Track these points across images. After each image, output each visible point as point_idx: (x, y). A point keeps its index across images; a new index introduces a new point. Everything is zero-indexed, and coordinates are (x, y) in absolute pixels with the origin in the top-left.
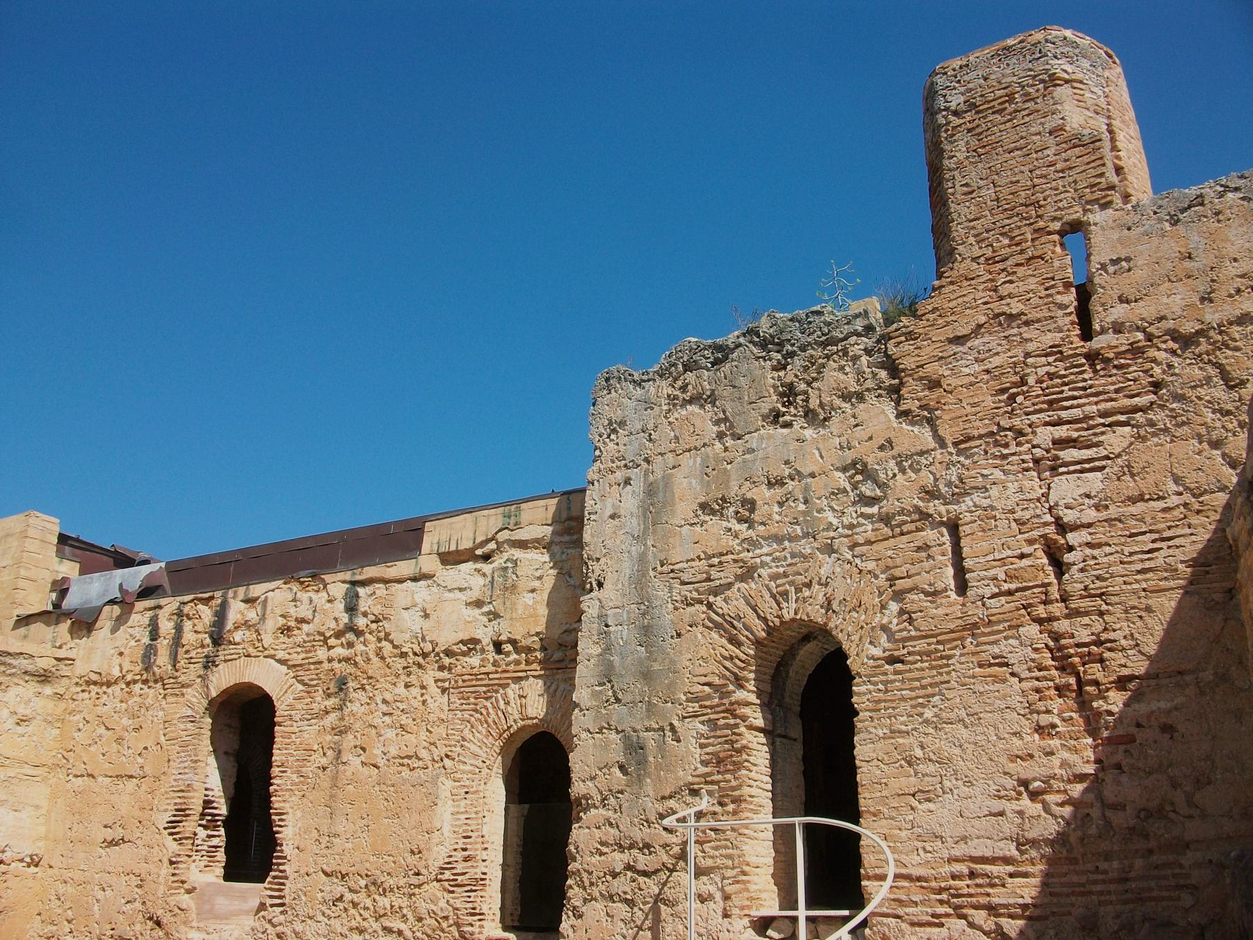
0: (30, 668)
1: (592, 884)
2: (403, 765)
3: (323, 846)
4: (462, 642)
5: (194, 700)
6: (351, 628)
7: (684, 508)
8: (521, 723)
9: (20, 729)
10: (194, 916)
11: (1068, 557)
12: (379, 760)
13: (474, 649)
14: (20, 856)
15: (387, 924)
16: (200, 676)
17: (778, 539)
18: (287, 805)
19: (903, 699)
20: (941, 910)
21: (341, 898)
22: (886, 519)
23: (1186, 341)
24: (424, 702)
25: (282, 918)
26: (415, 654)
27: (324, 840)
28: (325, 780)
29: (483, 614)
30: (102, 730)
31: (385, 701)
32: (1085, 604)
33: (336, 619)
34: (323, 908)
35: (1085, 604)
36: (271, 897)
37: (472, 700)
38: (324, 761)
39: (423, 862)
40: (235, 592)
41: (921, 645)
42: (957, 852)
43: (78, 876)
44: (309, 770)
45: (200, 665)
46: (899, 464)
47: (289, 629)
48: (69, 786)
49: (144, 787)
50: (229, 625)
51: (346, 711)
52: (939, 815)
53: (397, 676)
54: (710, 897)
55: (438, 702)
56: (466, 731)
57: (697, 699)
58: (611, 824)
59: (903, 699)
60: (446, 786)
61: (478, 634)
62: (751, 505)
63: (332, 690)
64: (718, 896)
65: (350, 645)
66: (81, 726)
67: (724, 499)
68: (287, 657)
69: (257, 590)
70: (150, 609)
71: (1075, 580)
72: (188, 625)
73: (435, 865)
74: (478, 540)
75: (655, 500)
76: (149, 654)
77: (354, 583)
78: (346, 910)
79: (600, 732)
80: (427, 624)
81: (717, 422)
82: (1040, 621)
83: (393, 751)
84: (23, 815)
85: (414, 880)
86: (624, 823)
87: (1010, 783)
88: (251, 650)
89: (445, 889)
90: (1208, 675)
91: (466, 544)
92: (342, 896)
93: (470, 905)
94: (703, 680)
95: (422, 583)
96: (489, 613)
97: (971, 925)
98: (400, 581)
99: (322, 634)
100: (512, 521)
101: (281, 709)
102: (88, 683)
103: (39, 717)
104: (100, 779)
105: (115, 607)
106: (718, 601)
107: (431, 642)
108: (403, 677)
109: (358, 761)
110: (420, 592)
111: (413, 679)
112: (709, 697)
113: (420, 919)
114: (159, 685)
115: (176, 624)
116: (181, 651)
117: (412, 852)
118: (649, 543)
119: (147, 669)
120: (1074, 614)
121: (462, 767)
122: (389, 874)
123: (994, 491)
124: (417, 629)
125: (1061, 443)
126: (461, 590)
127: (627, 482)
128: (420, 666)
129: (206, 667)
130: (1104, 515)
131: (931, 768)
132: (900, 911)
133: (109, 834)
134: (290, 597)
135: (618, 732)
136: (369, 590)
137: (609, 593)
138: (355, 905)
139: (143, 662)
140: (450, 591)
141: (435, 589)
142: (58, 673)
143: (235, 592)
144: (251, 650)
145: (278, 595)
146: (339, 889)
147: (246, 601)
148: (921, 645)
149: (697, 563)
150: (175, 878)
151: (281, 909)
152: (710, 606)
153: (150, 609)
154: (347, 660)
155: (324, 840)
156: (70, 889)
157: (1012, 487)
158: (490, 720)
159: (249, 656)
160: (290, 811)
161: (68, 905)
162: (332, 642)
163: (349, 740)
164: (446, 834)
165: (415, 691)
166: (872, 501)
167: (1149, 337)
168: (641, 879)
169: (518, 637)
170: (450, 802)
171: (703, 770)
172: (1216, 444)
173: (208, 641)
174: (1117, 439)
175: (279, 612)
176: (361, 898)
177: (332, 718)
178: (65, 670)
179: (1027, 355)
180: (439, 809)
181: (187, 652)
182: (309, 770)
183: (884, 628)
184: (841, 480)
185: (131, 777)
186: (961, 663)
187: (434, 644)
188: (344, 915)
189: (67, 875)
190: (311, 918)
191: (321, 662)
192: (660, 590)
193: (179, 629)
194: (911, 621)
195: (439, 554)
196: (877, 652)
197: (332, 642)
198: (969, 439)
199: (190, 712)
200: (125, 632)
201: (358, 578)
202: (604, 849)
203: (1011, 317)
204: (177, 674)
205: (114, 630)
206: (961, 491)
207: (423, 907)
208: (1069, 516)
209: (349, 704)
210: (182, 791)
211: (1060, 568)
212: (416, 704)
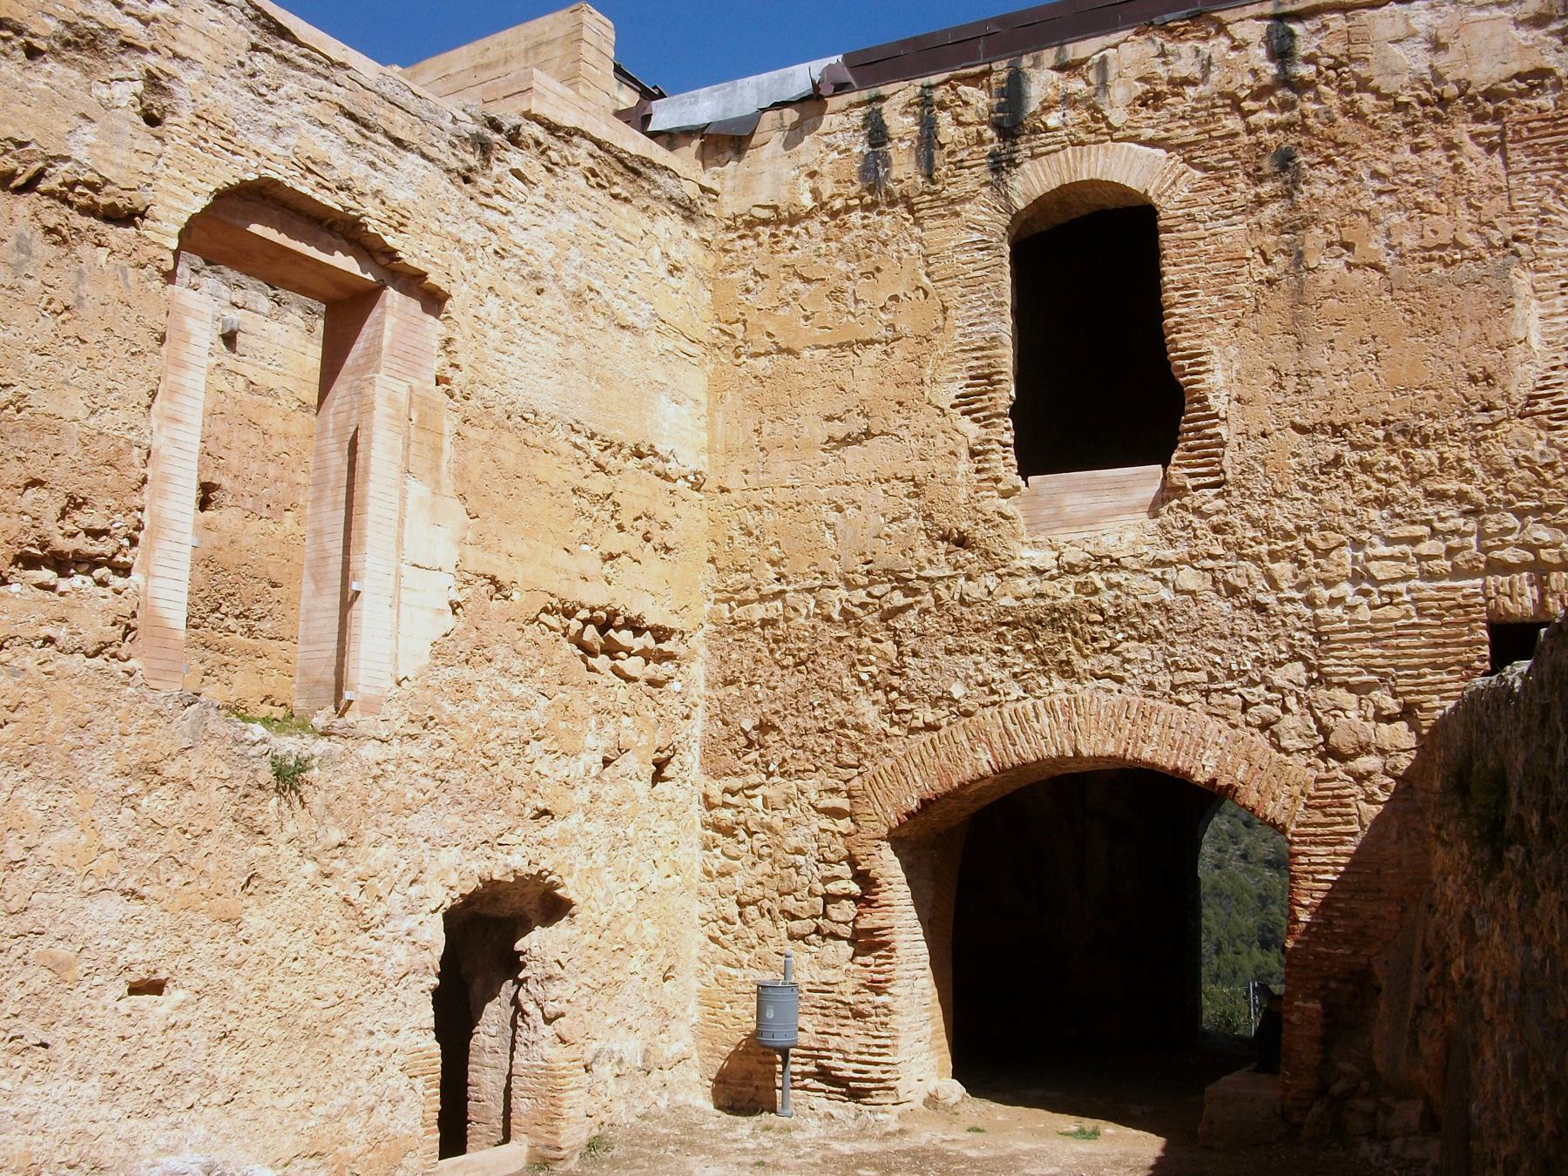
0: (676, 193)
2: (1431, 259)
3: (1290, 390)
5: (982, 217)
6: (1285, 81)
10: (1022, 528)
13: (1541, 86)
14: (685, 471)
15: (1432, 486)
16: (986, 184)
24: (1456, 168)
25: (1221, 503)
27: (1291, 384)
28: (1279, 301)
30: (797, 284)
31: (1375, 175)
37: (1554, 155)
38: (1268, 272)
39: (1499, 391)
40: (1036, 59)
43: (782, 496)
44: (1241, 286)
45: (984, 168)
47: (1158, 96)
48: (742, 371)
49: (898, 353)
50: (1033, 105)
51: (1300, 198)
55: (1479, 165)
60: (1523, 280)
65: (1286, 106)
68: (1164, 135)
70: (860, 104)
72: (944, 118)
76: (873, 170)
77: (1279, 18)
78: (1348, 476)
83: (1409, 241)
89: (1541, 426)
101: (1168, 210)
102: (750, 224)
104: (806, 354)
105: (787, 111)
107: (1457, 82)
108: (1406, 138)
111: (1426, 138)
113: (1500, 473)
114: (900, 209)
116: (939, 157)
119: (871, 190)
122: (1430, 415)
128: (1437, 119)
134: (1154, 50)
138: (1365, 467)
139: (863, 178)
142: (702, 210)
143: (1036, 59)
144: (1083, 136)
146: (1329, 450)
147: (1060, 68)
150: (984, 476)
154: (1288, 127)
155: (1291, 384)
159: (1082, 143)
160: (1215, 349)
161: (770, 539)
162: (1248, 105)
163: (1315, 237)
170: (1534, 303)
173: (989, 133)
176: (1380, 456)
178: (709, 209)
180: (1519, 312)
181: (952, 153)
182: (1241, 286)
185: (871, 342)
188: (1346, 485)
189: (758, 498)
193: (928, 128)
199: (976, 236)
200: (816, 141)
204: (939, 187)
205: (789, 144)
207: (1505, 456)
210: (982, 349)
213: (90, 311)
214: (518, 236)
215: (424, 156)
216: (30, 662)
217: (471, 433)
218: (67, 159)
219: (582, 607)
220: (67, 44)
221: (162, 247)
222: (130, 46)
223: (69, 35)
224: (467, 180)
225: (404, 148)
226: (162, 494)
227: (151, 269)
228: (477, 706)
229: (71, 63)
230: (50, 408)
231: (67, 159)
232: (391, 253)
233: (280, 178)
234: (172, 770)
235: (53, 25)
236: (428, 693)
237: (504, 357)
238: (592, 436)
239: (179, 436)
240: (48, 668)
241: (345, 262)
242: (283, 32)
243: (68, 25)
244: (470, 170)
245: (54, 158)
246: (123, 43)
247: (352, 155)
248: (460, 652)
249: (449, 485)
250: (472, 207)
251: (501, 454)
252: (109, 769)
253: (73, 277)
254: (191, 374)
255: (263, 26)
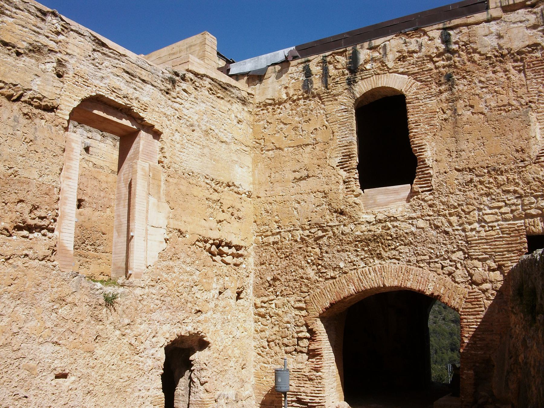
0: (239, 95)
2: (501, 110)
3: (454, 157)
5: (345, 101)
6: (448, 50)
9: (239, 126)
12: (484, 110)
13: (536, 49)
14: (245, 191)
16: (346, 89)
25: (431, 197)
27: (454, 155)
28: (449, 126)
30: (282, 126)
31: (480, 81)
33: (437, 48)
34: (460, 188)
36: (421, 187)
43: (279, 199)
44: (436, 121)
47: (404, 57)
48: (264, 156)
50: (361, 62)
51: (455, 91)
55: (516, 77)
60: (533, 116)
63: (443, 81)
65: (449, 59)
66: (266, 126)
69: (377, 42)
70: (301, 63)
72: (331, 67)
77: (445, 29)
78: (475, 186)
83: (493, 104)
84: (244, 170)
88: (379, 71)
99: (430, 56)
101: (409, 96)
102: (265, 105)
103: (245, 121)
104: (286, 149)
105: (276, 66)
107: (507, 49)
110: (494, 27)
111: (497, 68)
113: (528, 183)
114: (317, 99)
115: (323, 67)
116: (330, 80)
119: (306, 92)
122: (503, 164)
129: (349, 84)
133: (297, 175)
134: (402, 42)
136: (457, 31)
139: (303, 88)
140: (514, 23)
141: (503, 24)
144: (379, 71)
145: (394, 44)
146: (468, 177)
147: (370, 48)
153: (301, 63)
154: (449, 66)
155: (454, 155)
156: (275, 207)
159: (379, 74)
160: (427, 143)
161: (275, 214)
170: (538, 124)
175: (395, 50)
176: (486, 178)
180: (532, 127)
181: (334, 79)
182: (436, 121)
185: (308, 145)
188: (475, 189)
189: (271, 200)
190: (452, 193)
193: (325, 71)
199: (343, 107)
200: (287, 76)
201: (448, 26)
204: (330, 91)
205: (278, 77)
207: (530, 177)
210: (346, 146)
213: (39, 141)
214: (185, 112)
215: (153, 85)
216: (20, 263)
217: (171, 180)
218: (31, 90)
219: (210, 239)
220: (30, 51)
221: (63, 119)
222: (52, 51)
223: (31, 48)
224: (167, 93)
225: (146, 83)
226: (65, 204)
227: (60, 126)
228: (175, 275)
229: (32, 57)
230: (26, 175)
231: (31, 90)
232: (142, 119)
233: (104, 94)
234: (69, 299)
235: (25, 44)
236: (158, 270)
237: (181, 153)
238: (213, 180)
239: (70, 184)
240: (26, 265)
241: (126, 122)
242: (104, 45)
243: (31, 44)
244: (168, 89)
245: (26, 90)
246: (49, 50)
247: (128, 86)
248: (169, 256)
249: (163, 198)
250: (169, 102)
251: (181, 187)
252: (48, 300)
253: (33, 130)
254: (74, 162)
255: (97, 43)
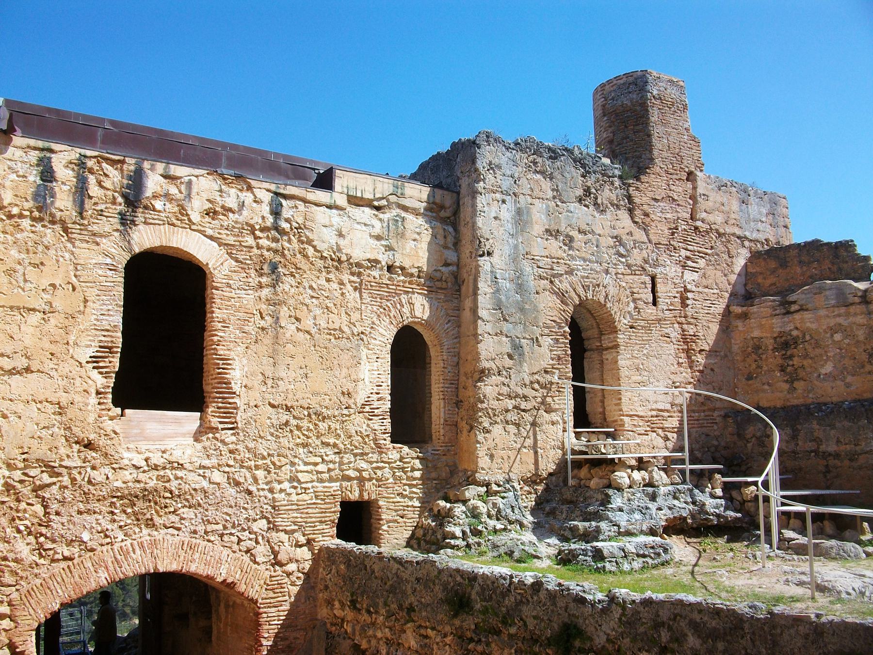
1: (495, 415)
2: (330, 334)
3: (269, 386)
4: (368, 260)
5: (113, 250)
6: (276, 228)
7: (538, 229)
8: (410, 320)
11: (688, 302)
15: (325, 440)
17: (585, 260)
18: (232, 353)
19: (636, 344)
20: (648, 429)
21: (287, 423)
22: (629, 266)
23: (720, 235)
24: (343, 294)
25: (234, 439)
26: (332, 260)
29: (382, 245)
31: (311, 287)
32: (692, 320)
33: (263, 218)
35: (692, 320)
36: (221, 423)
37: (378, 300)
41: (642, 323)
42: (654, 407)
46: (634, 244)
52: (648, 392)
53: (320, 271)
54: (558, 422)
56: (375, 319)
57: (548, 327)
58: (504, 384)
59: (636, 344)
60: (364, 352)
61: (380, 257)
62: (571, 239)
64: (561, 421)
67: (558, 231)
71: (690, 311)
73: (360, 400)
74: (377, 196)
75: (521, 217)
79: (496, 335)
80: (342, 242)
81: (553, 190)
82: (679, 323)
85: (345, 412)
86: (512, 385)
87: (671, 383)
90: (722, 354)
91: (368, 195)
92: (287, 422)
93: (384, 428)
94: (552, 318)
95: (334, 211)
96: (386, 246)
97: (658, 435)
98: (317, 205)
100: (399, 191)
106: (557, 281)
107: (347, 255)
109: (293, 327)
112: (554, 327)
117: (343, 393)
118: (520, 241)
120: (689, 323)
121: (373, 341)
123: (668, 268)
124: (333, 242)
125: (688, 258)
126: (365, 225)
127: (504, 202)
128: (337, 269)
130: (698, 289)
131: (646, 373)
132: (634, 429)
135: (507, 336)
136: (291, 203)
137: (496, 259)
140: (358, 223)
145: (205, 186)
146: (284, 417)
147: (165, 177)
148: (642, 323)
149: (545, 259)
150: (103, 407)
151: (232, 432)
152: (551, 282)
155: (270, 382)
157: (673, 269)
158: (392, 315)
163: (284, 311)
164: (367, 383)
165: (335, 286)
166: (622, 256)
167: (711, 229)
168: (523, 413)
169: (407, 266)
171: (551, 362)
172: (725, 275)
174: (702, 263)
177: (266, 292)
179: (678, 218)
180: (362, 367)
181: (96, 204)
183: (629, 312)
184: (611, 242)
186: (656, 333)
187: (349, 258)
191: (252, 248)
192: (527, 268)
194: (639, 312)
195: (348, 196)
196: (626, 322)
197: (258, 233)
198: (660, 244)
201: (282, 191)
202: (501, 398)
203: (674, 200)
206: (656, 265)
208: (689, 287)
209: (281, 284)
210: (108, 331)
211: (684, 305)
212: (337, 294)
